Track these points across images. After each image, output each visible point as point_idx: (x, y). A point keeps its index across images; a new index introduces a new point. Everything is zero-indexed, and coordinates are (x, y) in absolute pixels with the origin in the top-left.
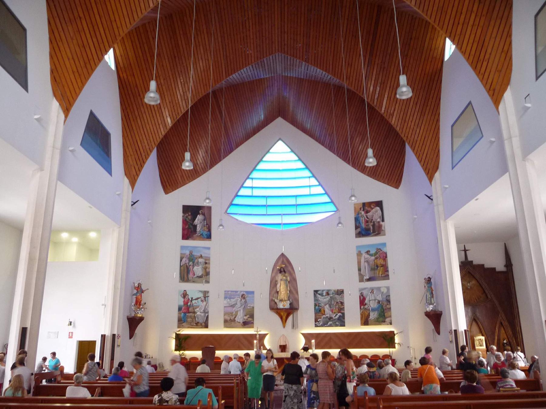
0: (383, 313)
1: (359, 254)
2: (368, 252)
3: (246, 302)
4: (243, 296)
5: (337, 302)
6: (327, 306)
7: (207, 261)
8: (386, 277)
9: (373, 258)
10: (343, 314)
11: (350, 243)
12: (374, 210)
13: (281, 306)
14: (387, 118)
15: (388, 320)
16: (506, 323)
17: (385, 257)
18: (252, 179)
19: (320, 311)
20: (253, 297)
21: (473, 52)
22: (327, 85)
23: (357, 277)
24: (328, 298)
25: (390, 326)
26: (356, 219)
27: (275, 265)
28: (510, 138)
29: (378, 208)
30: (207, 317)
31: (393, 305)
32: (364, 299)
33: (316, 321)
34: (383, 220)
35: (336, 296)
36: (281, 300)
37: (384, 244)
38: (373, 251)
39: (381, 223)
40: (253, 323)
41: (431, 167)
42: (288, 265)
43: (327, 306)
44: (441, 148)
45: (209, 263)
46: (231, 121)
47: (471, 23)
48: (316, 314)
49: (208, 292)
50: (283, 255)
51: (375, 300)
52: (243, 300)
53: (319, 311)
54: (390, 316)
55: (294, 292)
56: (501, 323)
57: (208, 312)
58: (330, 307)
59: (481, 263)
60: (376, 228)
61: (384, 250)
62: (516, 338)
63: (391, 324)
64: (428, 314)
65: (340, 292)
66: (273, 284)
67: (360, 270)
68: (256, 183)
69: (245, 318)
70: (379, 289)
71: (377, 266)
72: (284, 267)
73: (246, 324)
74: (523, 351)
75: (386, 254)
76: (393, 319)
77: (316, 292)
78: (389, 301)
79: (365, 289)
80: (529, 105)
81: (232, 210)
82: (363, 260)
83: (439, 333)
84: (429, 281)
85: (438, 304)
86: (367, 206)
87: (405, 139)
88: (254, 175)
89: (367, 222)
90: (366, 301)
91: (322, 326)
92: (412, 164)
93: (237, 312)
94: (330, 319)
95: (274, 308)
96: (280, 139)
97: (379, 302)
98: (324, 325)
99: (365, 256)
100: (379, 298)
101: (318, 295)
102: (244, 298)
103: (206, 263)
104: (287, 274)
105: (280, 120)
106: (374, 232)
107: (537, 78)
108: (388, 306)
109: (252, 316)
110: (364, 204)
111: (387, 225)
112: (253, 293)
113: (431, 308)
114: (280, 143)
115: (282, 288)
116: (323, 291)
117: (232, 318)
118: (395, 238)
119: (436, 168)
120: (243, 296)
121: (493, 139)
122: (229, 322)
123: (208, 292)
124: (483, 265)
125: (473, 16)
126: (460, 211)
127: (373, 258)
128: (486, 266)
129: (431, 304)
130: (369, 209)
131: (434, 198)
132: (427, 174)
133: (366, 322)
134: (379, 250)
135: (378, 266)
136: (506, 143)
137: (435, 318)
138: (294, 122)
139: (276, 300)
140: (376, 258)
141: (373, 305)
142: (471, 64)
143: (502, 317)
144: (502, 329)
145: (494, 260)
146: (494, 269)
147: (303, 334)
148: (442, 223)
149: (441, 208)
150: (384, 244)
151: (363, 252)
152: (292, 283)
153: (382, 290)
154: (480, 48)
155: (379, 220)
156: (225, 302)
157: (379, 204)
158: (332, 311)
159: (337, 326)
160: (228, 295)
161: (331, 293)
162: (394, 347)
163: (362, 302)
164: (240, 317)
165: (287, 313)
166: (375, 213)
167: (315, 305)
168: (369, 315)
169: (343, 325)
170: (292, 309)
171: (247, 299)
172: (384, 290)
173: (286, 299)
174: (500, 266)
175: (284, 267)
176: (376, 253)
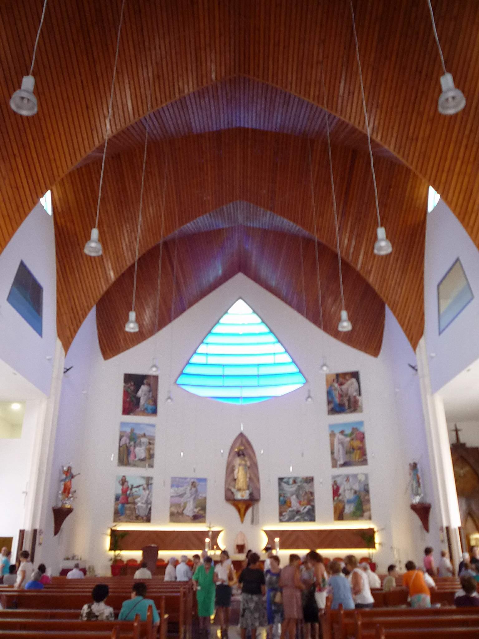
0: (361, 508)
1: (332, 435)
2: (342, 432)
4: (193, 484)
5: (306, 493)
7: (151, 441)
8: (364, 462)
9: (348, 439)
10: (313, 507)
11: (322, 421)
12: (349, 382)
13: (239, 496)
15: (366, 514)
17: (362, 438)
20: (206, 485)
24: (294, 488)
25: (368, 521)
27: (232, 448)
29: (354, 380)
30: (150, 509)
33: (281, 514)
34: (360, 394)
35: (305, 484)
36: (239, 490)
37: (361, 423)
38: (348, 431)
39: (358, 398)
40: (204, 517)
41: (415, 332)
43: (294, 497)
45: (153, 444)
49: (152, 478)
50: (241, 435)
51: (351, 489)
52: (194, 489)
53: (284, 503)
54: (369, 510)
55: (255, 480)
57: (150, 503)
58: (297, 498)
61: (362, 429)
63: (370, 518)
64: (414, 508)
65: (310, 480)
66: (230, 469)
67: (332, 453)
69: (196, 510)
70: (355, 476)
71: (353, 449)
72: (243, 449)
73: (197, 518)
77: (281, 480)
78: (367, 491)
79: (338, 476)
82: (336, 442)
84: (414, 467)
85: (425, 494)
86: (341, 378)
87: (384, 299)
89: (341, 396)
90: (341, 491)
92: (392, 327)
93: (186, 504)
94: (298, 512)
95: (230, 499)
96: (240, 298)
97: (355, 492)
98: (291, 519)
99: (339, 436)
100: (356, 487)
101: (284, 486)
102: (195, 487)
103: (150, 444)
104: (246, 458)
106: (349, 407)
108: (366, 498)
109: (204, 508)
110: (338, 375)
111: (364, 400)
112: (205, 480)
115: (240, 474)
116: (289, 478)
117: (180, 511)
118: (374, 417)
119: (420, 333)
120: (193, 484)
122: (175, 517)
123: (152, 478)
127: (348, 439)
129: (417, 494)
130: (344, 381)
131: (419, 368)
133: (340, 516)
134: (354, 430)
135: (354, 450)
137: (423, 511)
140: (352, 439)
141: (348, 495)
148: (428, 397)
150: (361, 423)
151: (337, 432)
152: (253, 469)
155: (355, 394)
157: (355, 375)
159: (305, 521)
160: (176, 483)
161: (298, 481)
163: (336, 492)
164: (190, 510)
165: (245, 506)
166: (350, 386)
167: (280, 496)
168: (343, 509)
169: (312, 519)
172: (362, 478)
173: (245, 487)
175: (243, 449)
176: (352, 433)
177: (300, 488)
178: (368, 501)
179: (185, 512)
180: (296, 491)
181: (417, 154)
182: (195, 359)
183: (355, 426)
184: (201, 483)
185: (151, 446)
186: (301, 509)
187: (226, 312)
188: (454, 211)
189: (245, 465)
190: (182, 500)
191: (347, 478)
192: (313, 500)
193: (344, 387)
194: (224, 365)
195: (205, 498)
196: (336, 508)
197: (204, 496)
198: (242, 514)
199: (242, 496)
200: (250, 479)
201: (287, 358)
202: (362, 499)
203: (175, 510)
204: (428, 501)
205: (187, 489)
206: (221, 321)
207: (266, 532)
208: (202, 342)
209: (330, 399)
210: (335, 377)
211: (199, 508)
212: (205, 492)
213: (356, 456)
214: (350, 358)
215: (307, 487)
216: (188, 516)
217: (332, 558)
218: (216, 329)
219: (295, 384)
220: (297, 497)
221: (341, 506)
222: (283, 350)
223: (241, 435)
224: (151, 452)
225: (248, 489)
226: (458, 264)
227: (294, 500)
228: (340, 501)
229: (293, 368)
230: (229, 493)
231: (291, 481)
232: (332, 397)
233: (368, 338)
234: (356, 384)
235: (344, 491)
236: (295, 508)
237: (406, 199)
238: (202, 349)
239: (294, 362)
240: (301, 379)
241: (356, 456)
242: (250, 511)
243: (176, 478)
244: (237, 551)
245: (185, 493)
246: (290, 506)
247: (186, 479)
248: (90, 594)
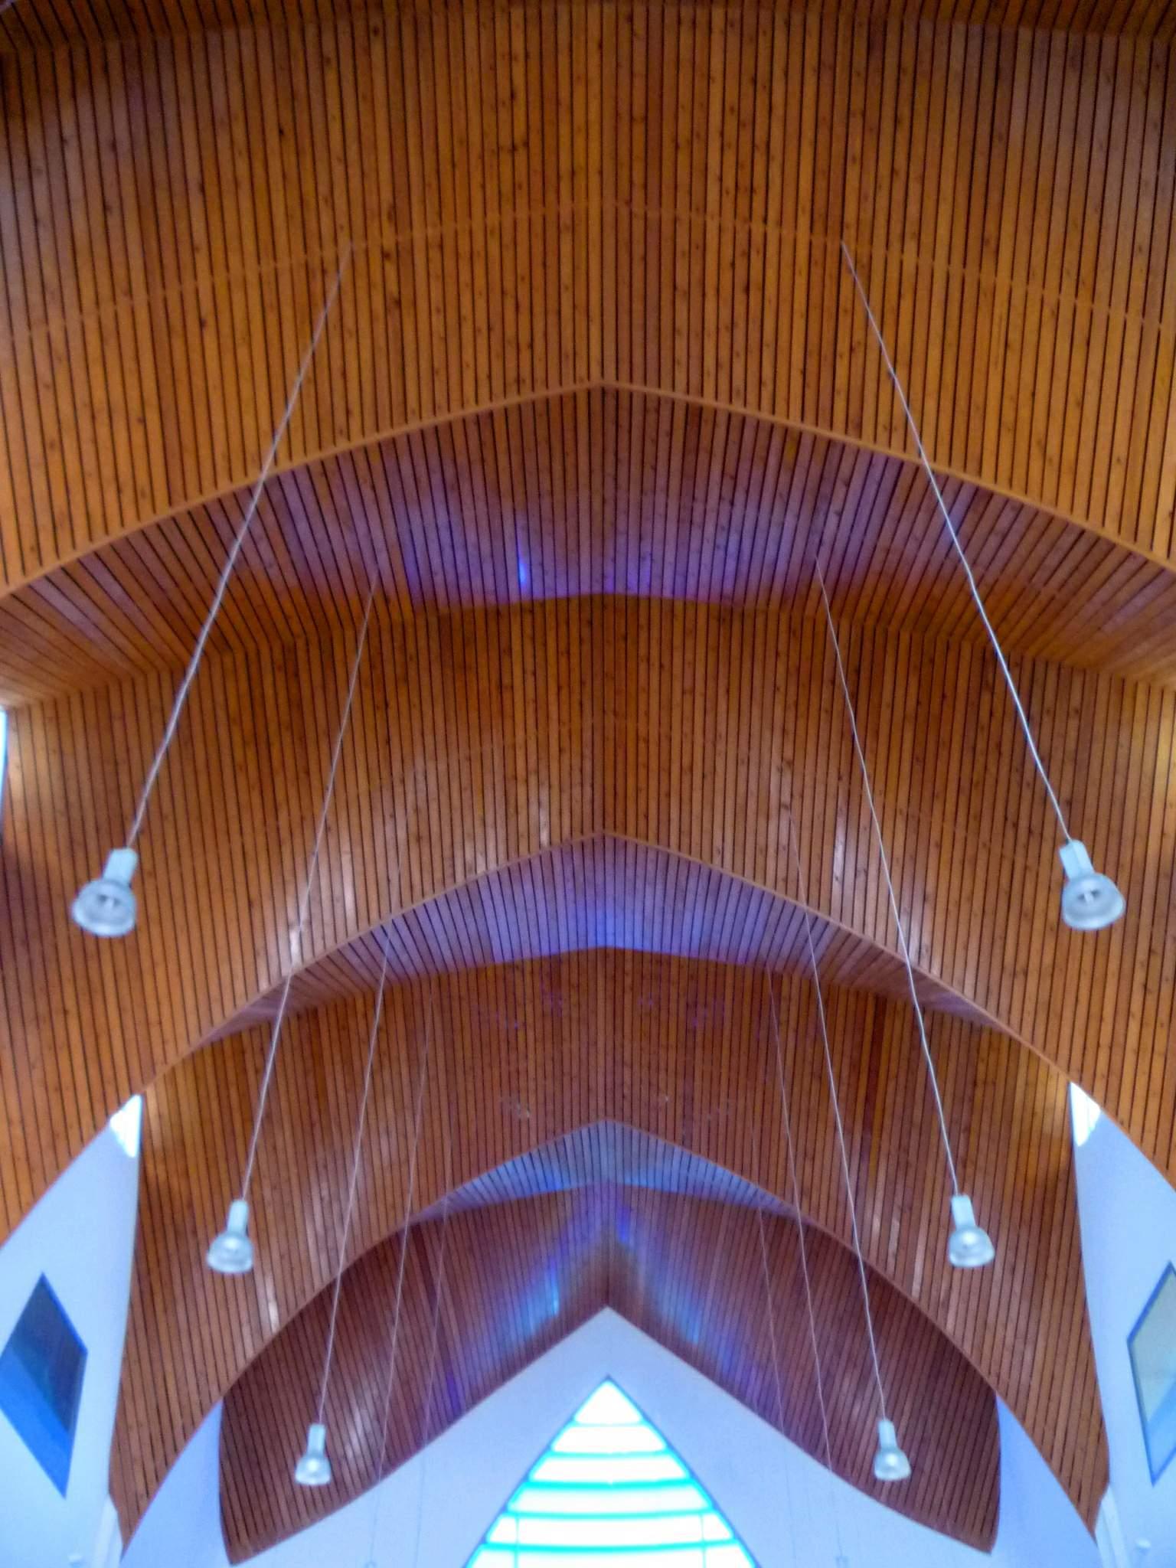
14: (931, 1315)
41: (1085, 1480)
88: (527, 1500)
132: (1077, 1500)
138: (650, 1325)
187: (570, 1420)
208: (504, 1509)
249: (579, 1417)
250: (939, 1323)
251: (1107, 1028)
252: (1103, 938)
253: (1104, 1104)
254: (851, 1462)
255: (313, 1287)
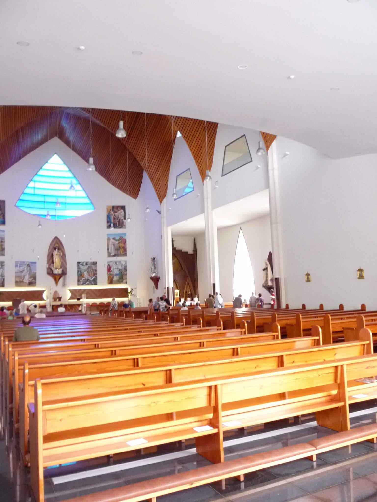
0: (122, 277)
1: (109, 239)
2: (114, 239)
3: (30, 269)
4: (29, 265)
5: (93, 270)
6: (86, 272)
7: (3, 241)
8: (125, 254)
9: (117, 242)
10: (97, 277)
11: (103, 233)
12: (120, 211)
13: (56, 272)
14: (139, 161)
15: (125, 281)
16: (190, 283)
17: (125, 242)
18: (35, 181)
19: (81, 275)
20: (36, 266)
21: (196, 151)
22: (101, 127)
23: (106, 254)
24: (86, 267)
25: (125, 284)
26: (108, 217)
27: (51, 244)
28: (207, 198)
29: (122, 211)
30: (4, 280)
31: (128, 272)
32: (110, 268)
33: (78, 281)
34: (125, 219)
35: (92, 266)
36: (56, 268)
37: (125, 234)
38: (117, 238)
39: (124, 220)
40: (35, 283)
41: (161, 194)
42: (60, 244)
43: (86, 272)
44: (168, 185)
45: (4, 242)
46: (23, 136)
47: (197, 136)
48: (78, 277)
49: (4, 262)
50: (56, 238)
51: (117, 269)
52: (29, 268)
53: (80, 275)
54: (126, 279)
55: (64, 263)
56: (188, 283)
57: (4, 276)
58: (87, 273)
59: (181, 249)
60: (120, 224)
61: (125, 238)
62: (195, 291)
63: (126, 283)
64: (152, 278)
65: (95, 263)
66: (51, 257)
67: (108, 249)
68: (37, 185)
69: (30, 280)
70: (120, 262)
71: (120, 248)
72: (57, 245)
73: (31, 284)
74: (198, 297)
75: (126, 240)
76: (128, 280)
77: (79, 263)
78: (126, 270)
79: (111, 261)
80: (217, 186)
81: (19, 204)
82: (110, 244)
83: (157, 289)
84: (154, 259)
85: (158, 273)
86: (115, 208)
87: (143, 167)
88: (36, 178)
89: (114, 219)
90: (112, 269)
91: (83, 284)
92: (147, 184)
93: (24, 276)
94: (88, 280)
95: (50, 272)
96: (56, 153)
97: (120, 270)
98: (84, 284)
99: (112, 240)
100: (120, 267)
101: (81, 266)
102: (29, 266)
103: (2, 242)
104: (60, 251)
105: (56, 140)
106: (119, 225)
107: (222, 176)
108: (125, 273)
109: (35, 278)
110: (113, 207)
111: (128, 222)
112: (35, 263)
113: (154, 275)
114: (56, 155)
115: (57, 259)
116: (83, 262)
117: (21, 280)
118: (132, 231)
119: (165, 196)
120: (29, 265)
121: (199, 195)
122: (19, 283)
123: (4, 262)
124: (181, 250)
125: (198, 133)
126: (176, 224)
127: (117, 242)
128: (183, 251)
129: (154, 272)
130: (117, 210)
131: (162, 212)
132: (159, 199)
133: (111, 282)
134: (121, 238)
135: (120, 248)
136: (205, 200)
137: (156, 280)
138: (67, 143)
139: (52, 268)
140: (120, 243)
141: (116, 272)
142: (194, 157)
143: (189, 279)
144: (188, 286)
145: (188, 248)
146: (187, 253)
147: (70, 290)
148: (165, 227)
149: (165, 220)
150: (125, 234)
151: (111, 238)
152: (63, 257)
153: (122, 262)
154: (199, 149)
155: (122, 218)
156: (16, 269)
157: (123, 208)
158: (89, 275)
159: (92, 284)
160: (18, 264)
161: (88, 263)
162: (128, 297)
163: (109, 269)
164: (27, 279)
165: (58, 277)
166: (120, 213)
167: (78, 271)
168: (113, 278)
169: (96, 283)
170: (64, 273)
171: (31, 267)
172: (124, 263)
173: (59, 267)
174: (190, 251)
175: (57, 245)
176: (120, 239)
177: (89, 267)
178: (126, 274)
179: (24, 281)
180: (87, 268)
181: (180, 124)
182: (27, 191)
183: (121, 236)
184: (33, 265)
185: (3, 243)
186: (90, 278)
187: (47, 162)
188: (193, 153)
189: (60, 255)
190: (22, 274)
191: (116, 263)
192: (97, 274)
193: (117, 214)
194: (45, 196)
195: (36, 273)
196: (109, 278)
197: (35, 271)
198: (57, 282)
199: (58, 272)
200: (62, 263)
201: (83, 194)
202: (123, 273)
203: (18, 280)
204: (159, 275)
205: (24, 268)
206: (44, 167)
207: (70, 290)
208: (32, 180)
209: (108, 220)
210: (112, 208)
211: (32, 279)
212: (35, 269)
213: (121, 251)
214: (120, 197)
215: (93, 267)
216: (26, 283)
217: (105, 303)
218: (41, 172)
219: (89, 210)
220: (88, 272)
221: (111, 277)
222: (81, 189)
223: (56, 238)
224: (3, 247)
225: (61, 268)
226: (189, 171)
227: (86, 274)
228: (112, 274)
229: (87, 201)
230: (49, 270)
231: (84, 264)
232: (110, 219)
233: (134, 190)
234: (123, 213)
235: (114, 269)
236: (86, 278)
237: (167, 127)
238: (31, 184)
239: (88, 196)
240: (91, 206)
241: (121, 251)
242: (61, 280)
243: (18, 262)
244: (53, 300)
245: (24, 270)
246: (84, 277)
247: (24, 262)
248: (271, 317)
249: (49, 161)
250: (140, 163)
251: (193, 132)
252: (200, 122)
253: (182, 134)
254: (87, 161)
255: (354, 395)
